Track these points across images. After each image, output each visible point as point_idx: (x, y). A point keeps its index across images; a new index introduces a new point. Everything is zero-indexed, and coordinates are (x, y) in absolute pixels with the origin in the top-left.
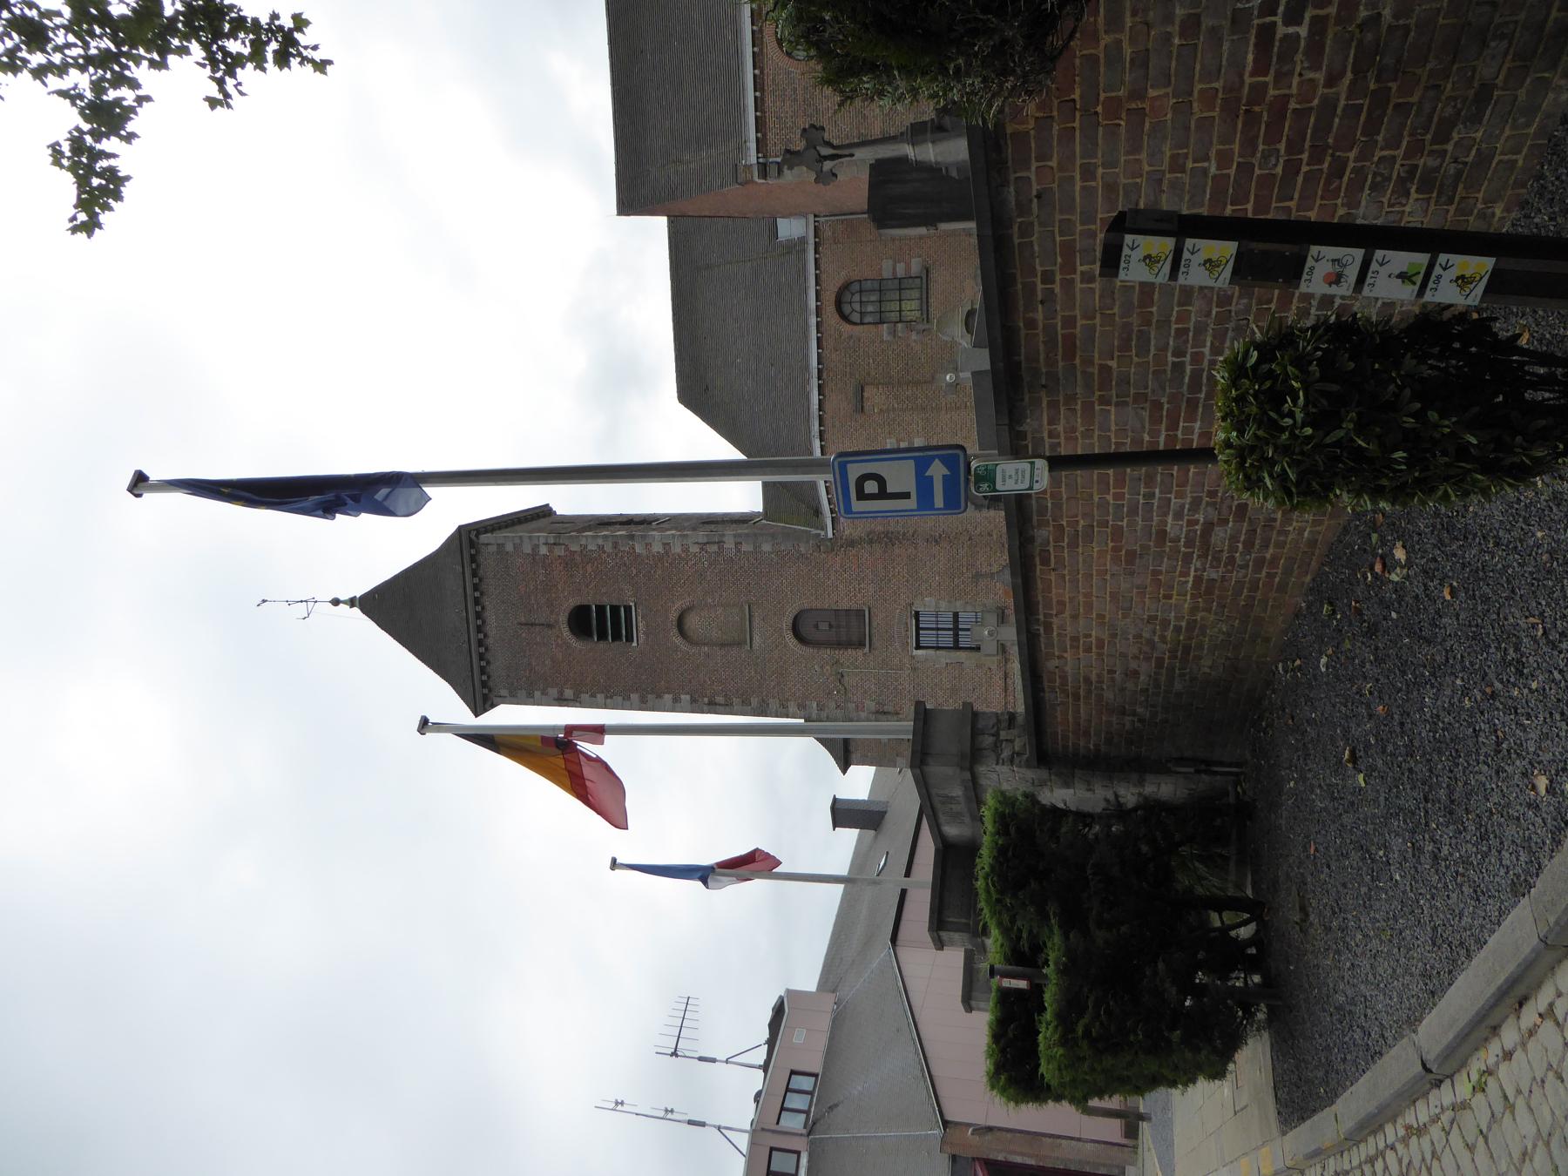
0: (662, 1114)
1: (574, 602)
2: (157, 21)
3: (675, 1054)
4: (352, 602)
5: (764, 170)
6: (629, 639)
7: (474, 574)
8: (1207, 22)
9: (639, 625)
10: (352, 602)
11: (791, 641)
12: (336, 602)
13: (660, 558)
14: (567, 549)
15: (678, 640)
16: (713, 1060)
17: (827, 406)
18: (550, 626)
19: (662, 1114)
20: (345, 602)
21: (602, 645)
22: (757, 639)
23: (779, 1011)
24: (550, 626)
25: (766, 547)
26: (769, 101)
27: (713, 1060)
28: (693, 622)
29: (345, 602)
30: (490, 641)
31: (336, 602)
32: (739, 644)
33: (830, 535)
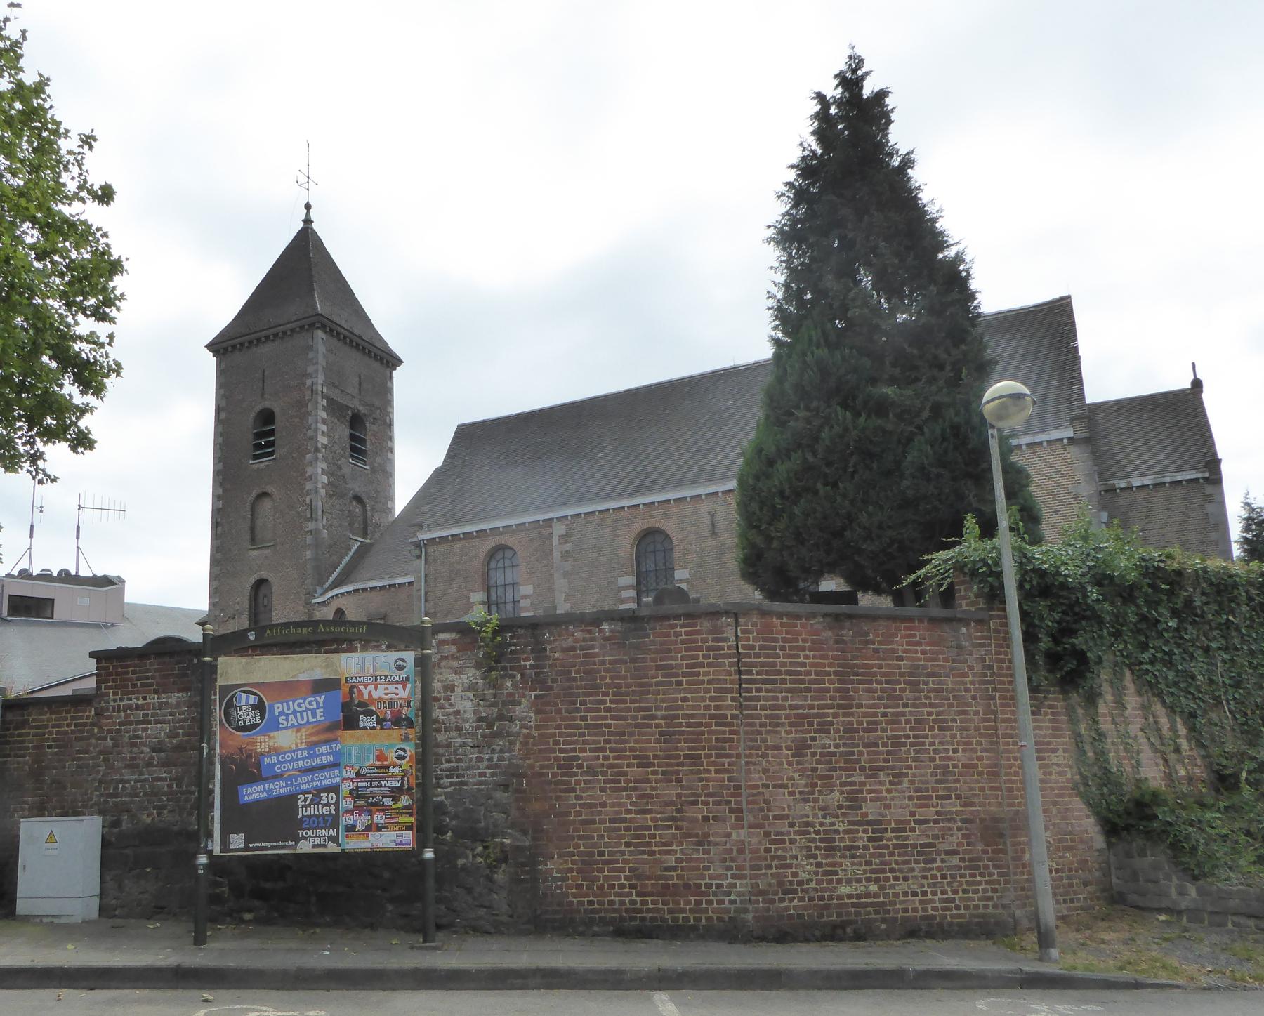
0: (37, 504)
1: (277, 411)
2: (51, 353)
3: (80, 507)
4: (308, 221)
5: (417, 545)
6: (256, 457)
7: (293, 330)
8: (995, 895)
9: (263, 463)
10: (308, 221)
11: (253, 579)
12: (308, 207)
13: (303, 474)
14: (309, 400)
15: (254, 494)
16: (78, 537)
17: (374, 593)
18: (262, 395)
19: (37, 504)
20: (308, 213)
21: (251, 437)
22: (255, 553)
23: (106, 581)
24: (262, 395)
25: (309, 554)
26: (459, 544)
27: (78, 537)
28: (267, 505)
29: (308, 213)
30: (254, 349)
31: (308, 207)
32: (253, 540)
33: (314, 601)
